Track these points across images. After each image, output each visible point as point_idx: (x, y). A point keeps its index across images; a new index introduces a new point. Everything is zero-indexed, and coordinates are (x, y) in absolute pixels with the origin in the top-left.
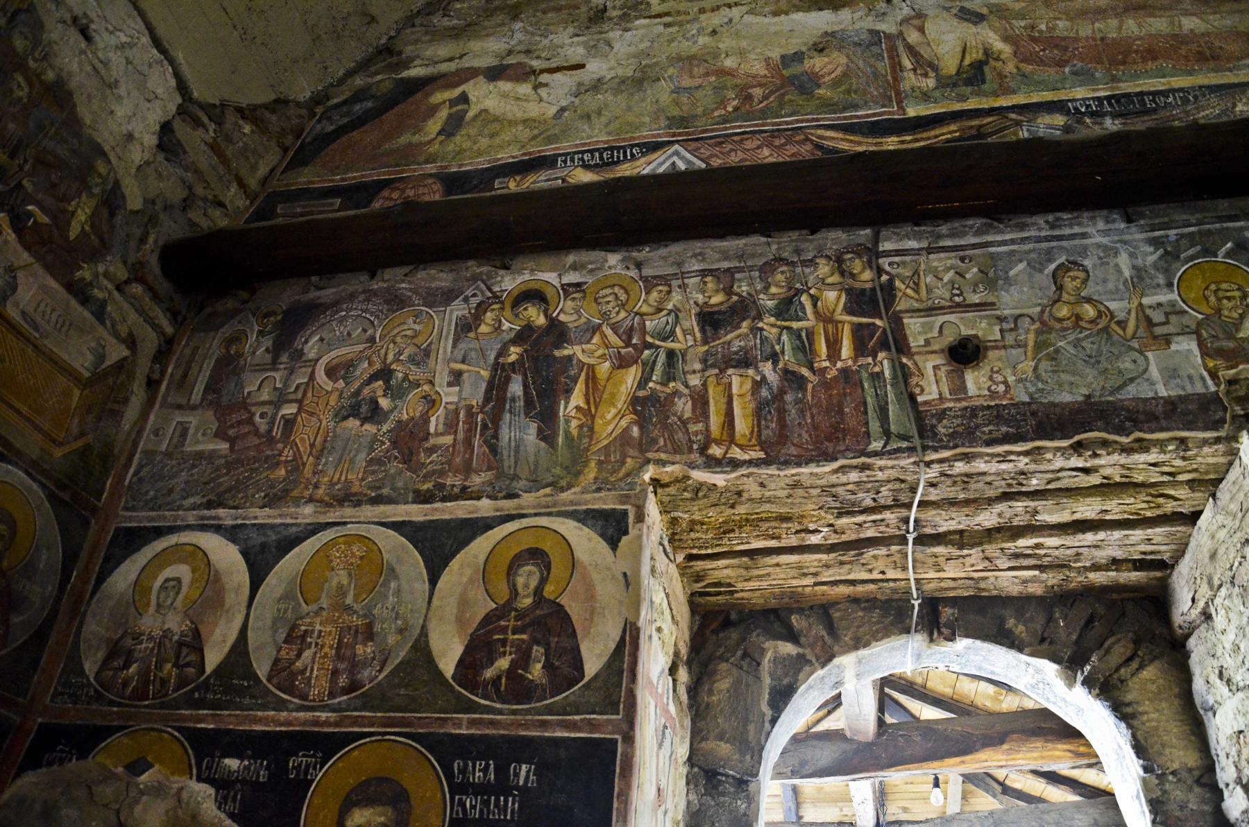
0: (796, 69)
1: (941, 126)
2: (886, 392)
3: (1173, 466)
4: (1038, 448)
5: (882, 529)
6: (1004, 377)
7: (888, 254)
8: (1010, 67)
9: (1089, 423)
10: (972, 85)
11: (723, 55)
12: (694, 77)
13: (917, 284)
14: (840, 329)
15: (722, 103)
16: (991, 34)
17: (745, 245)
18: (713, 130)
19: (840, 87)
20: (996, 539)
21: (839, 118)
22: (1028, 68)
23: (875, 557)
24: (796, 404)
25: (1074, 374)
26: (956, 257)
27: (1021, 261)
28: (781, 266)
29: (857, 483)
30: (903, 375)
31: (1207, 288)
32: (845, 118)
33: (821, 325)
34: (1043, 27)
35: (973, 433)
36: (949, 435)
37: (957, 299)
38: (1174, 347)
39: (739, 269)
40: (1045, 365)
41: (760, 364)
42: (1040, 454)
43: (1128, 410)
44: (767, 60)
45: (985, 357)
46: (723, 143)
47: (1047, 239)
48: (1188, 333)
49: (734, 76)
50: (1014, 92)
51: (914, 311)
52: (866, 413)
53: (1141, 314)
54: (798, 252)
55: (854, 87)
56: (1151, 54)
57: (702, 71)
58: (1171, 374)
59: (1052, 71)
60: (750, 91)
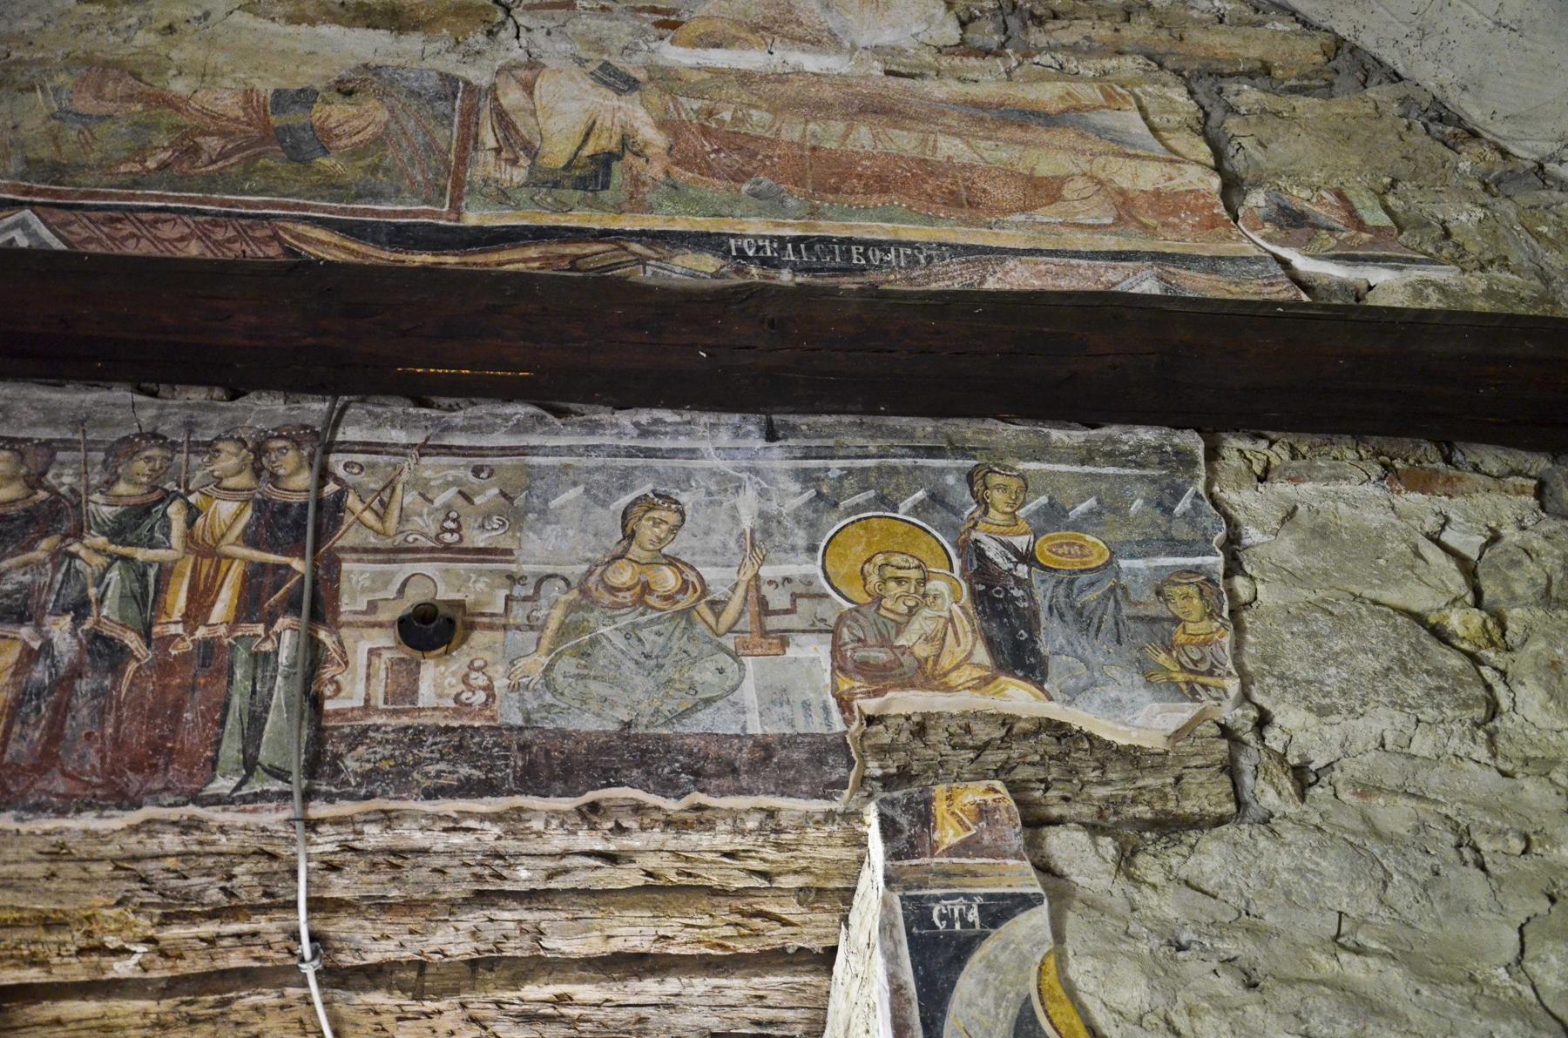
0: (295, 117)
1: (514, 247)
2: (271, 690)
3: (763, 860)
4: (520, 810)
5: (259, 951)
6: (490, 679)
7: (348, 447)
8: (656, 170)
9: (617, 771)
10: (585, 188)
11: (173, 72)
12: (102, 98)
13: (385, 505)
14: (224, 568)
15: (141, 153)
16: (641, 112)
17: (97, 403)
18: (106, 196)
19: (364, 158)
20: (485, 982)
21: (343, 211)
22: (682, 175)
23: (257, 1009)
24: (93, 698)
25: (614, 683)
26: (466, 466)
27: (575, 484)
28: (152, 447)
29: (183, 856)
30: (313, 659)
31: (869, 560)
32: (354, 212)
33: (191, 559)
34: (727, 116)
35: (407, 774)
36: (362, 775)
37: (448, 537)
38: (791, 652)
39: (68, 445)
40: (567, 664)
41: (48, 620)
42: (521, 820)
43: (690, 754)
44: (248, 94)
45: (464, 640)
46: (119, 220)
47: (631, 453)
48: (820, 631)
49: (178, 110)
50: (650, 209)
51: (366, 551)
52: (222, 723)
53: (753, 593)
54: (190, 426)
55: (386, 162)
56: (881, 183)
57: (121, 89)
58: (777, 697)
59: (721, 184)
60: (199, 140)
